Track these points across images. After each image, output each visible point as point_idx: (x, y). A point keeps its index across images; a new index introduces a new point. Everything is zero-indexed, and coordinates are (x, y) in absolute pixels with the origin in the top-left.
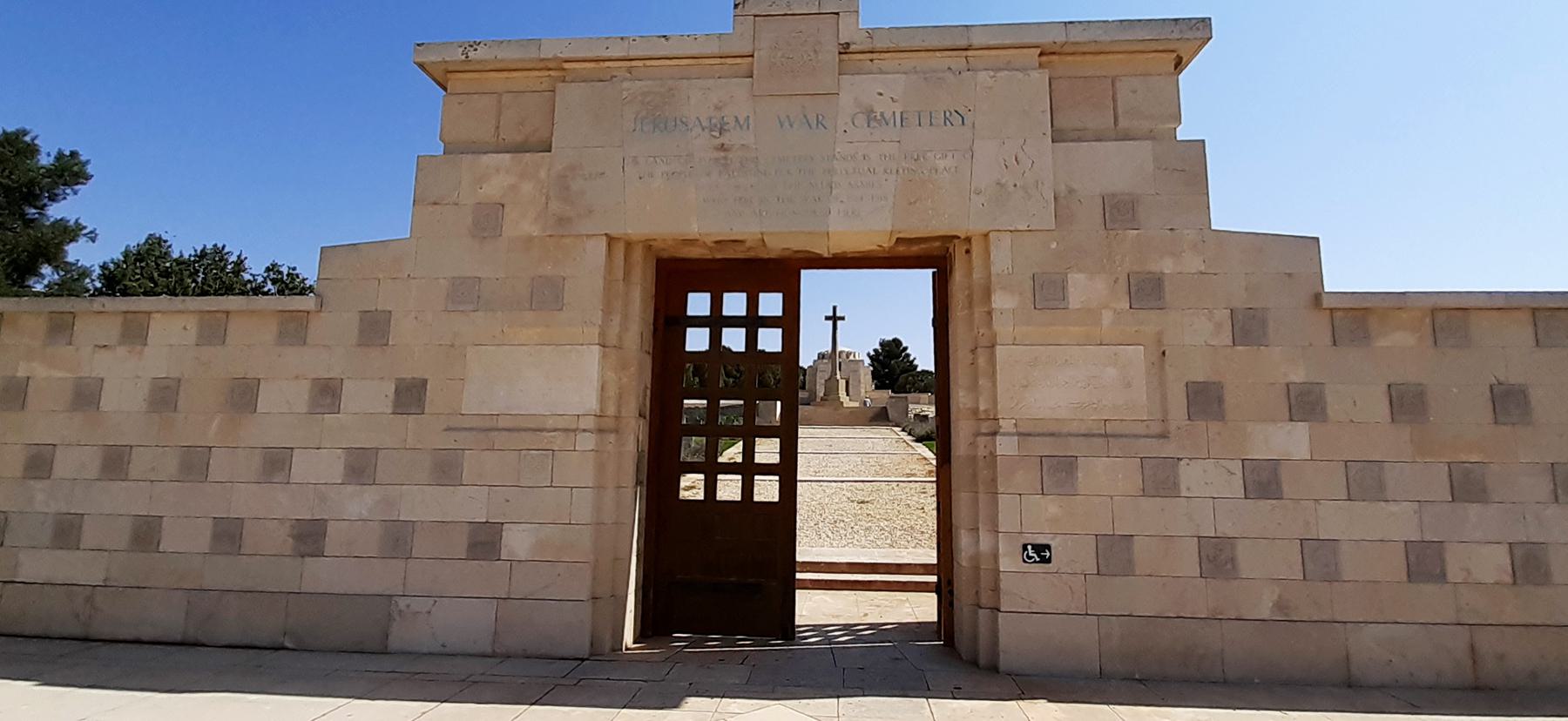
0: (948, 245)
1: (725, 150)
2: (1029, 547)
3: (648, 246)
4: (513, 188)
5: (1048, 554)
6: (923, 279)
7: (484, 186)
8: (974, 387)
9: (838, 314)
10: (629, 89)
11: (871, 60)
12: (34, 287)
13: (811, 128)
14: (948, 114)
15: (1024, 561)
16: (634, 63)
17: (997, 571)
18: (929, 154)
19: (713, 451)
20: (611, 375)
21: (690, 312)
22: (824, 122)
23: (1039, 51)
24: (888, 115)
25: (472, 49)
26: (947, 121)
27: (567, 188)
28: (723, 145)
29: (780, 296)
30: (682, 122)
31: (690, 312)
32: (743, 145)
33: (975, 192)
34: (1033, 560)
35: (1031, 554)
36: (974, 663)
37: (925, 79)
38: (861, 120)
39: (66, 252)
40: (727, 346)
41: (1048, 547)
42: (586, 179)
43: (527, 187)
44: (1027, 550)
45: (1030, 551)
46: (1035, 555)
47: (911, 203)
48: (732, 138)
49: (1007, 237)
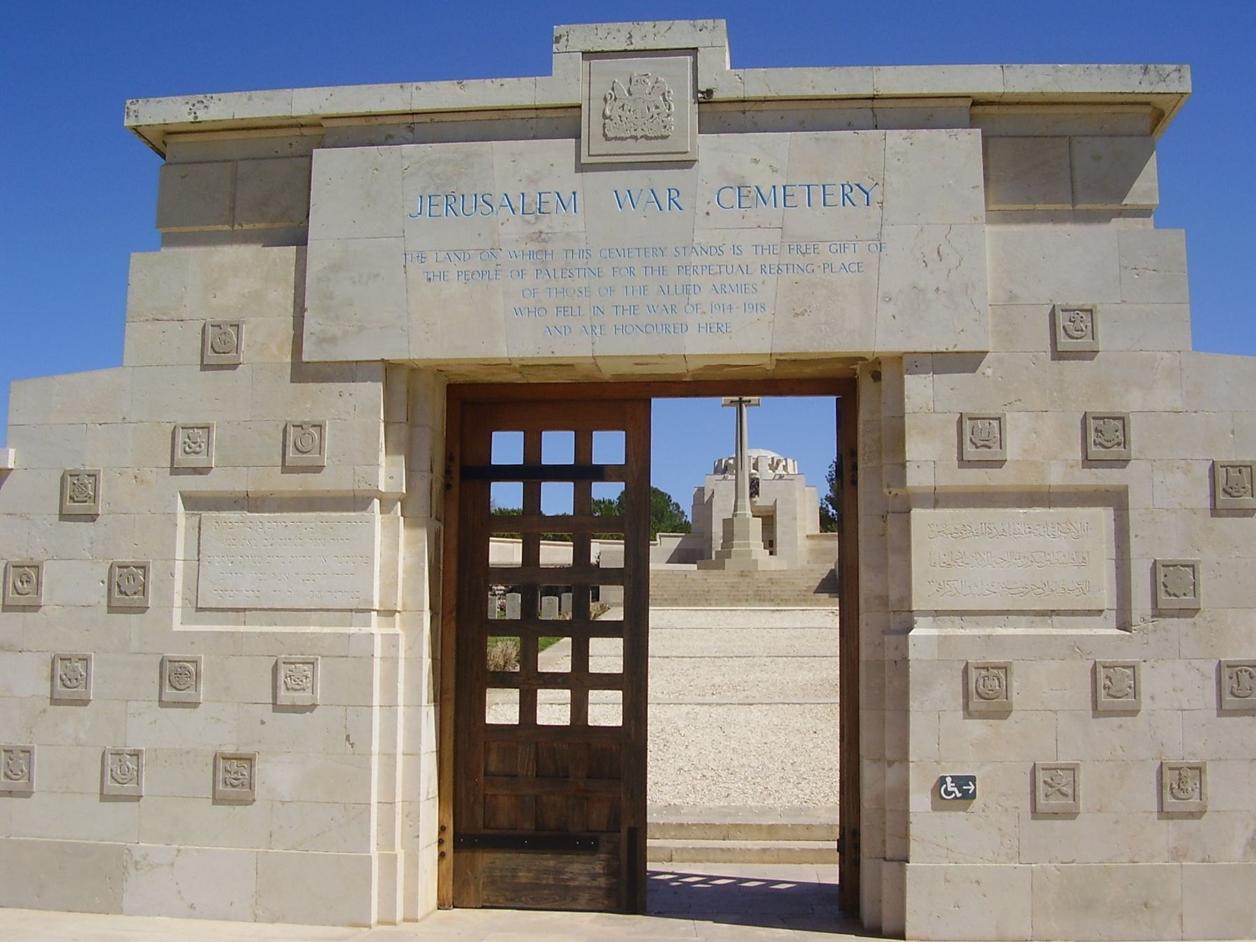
0: (854, 367)
1: (544, 241)
2: (949, 780)
3: (438, 370)
5: (972, 787)
6: (826, 406)
7: (218, 294)
11: (744, 112)
14: (847, 189)
16: (417, 119)
18: (821, 246)
19: (528, 656)
21: (547, 436)
23: (969, 102)
25: (202, 106)
29: (621, 435)
31: (547, 436)
32: (568, 234)
34: (954, 795)
35: (950, 789)
38: (730, 196)
40: (654, 487)
41: (973, 779)
42: (354, 282)
44: (946, 783)
45: (949, 784)
46: (955, 789)
48: (554, 223)
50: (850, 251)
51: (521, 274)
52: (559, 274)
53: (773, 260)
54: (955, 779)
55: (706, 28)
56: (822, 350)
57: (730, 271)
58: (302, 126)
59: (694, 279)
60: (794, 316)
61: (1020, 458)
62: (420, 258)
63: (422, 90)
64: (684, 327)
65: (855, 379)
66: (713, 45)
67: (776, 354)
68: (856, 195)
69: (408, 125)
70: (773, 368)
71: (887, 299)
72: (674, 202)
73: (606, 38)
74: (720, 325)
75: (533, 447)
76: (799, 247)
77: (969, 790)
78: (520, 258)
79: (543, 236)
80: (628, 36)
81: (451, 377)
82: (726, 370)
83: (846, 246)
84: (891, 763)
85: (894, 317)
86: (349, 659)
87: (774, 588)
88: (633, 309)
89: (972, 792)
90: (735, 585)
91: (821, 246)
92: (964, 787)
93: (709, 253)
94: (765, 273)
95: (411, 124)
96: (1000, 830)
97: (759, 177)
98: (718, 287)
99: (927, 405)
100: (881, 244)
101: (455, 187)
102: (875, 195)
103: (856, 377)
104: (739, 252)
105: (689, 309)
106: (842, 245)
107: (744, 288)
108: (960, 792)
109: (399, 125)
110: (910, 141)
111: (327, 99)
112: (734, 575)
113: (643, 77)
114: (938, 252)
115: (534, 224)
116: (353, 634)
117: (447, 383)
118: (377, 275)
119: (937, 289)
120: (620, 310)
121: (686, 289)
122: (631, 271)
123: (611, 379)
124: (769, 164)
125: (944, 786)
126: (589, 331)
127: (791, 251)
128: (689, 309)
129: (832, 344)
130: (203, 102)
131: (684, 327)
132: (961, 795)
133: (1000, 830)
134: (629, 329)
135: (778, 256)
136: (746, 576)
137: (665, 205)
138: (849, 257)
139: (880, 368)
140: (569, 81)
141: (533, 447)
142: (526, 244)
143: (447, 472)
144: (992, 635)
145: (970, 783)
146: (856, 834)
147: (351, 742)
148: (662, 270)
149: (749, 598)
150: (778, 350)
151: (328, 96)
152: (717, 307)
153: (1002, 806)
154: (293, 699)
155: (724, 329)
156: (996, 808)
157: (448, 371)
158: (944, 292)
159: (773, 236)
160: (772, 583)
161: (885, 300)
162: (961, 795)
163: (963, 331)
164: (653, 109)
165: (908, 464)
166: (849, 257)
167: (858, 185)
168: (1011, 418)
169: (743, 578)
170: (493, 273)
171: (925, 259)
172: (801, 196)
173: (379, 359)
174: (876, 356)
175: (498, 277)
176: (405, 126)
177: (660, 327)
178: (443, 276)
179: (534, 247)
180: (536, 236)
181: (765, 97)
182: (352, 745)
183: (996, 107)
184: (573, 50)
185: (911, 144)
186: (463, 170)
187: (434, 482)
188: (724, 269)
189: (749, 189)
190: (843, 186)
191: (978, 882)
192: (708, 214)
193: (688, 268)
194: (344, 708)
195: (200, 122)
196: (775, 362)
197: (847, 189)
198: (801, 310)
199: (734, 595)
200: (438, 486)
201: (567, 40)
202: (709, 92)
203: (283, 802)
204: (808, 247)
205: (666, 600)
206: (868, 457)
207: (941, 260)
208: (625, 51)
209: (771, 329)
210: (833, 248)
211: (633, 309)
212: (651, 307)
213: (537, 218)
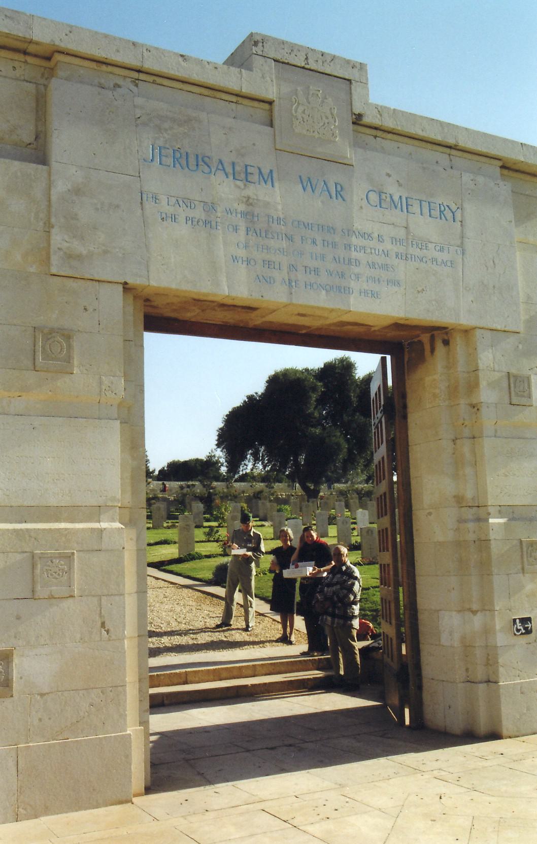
5: (530, 625)
12: (252, 597)
15: (515, 634)
18: (430, 245)
22: (341, 193)
23: (500, 163)
30: (203, 161)
35: (519, 628)
37: (424, 168)
39: (214, 574)
41: (529, 619)
44: (516, 624)
47: (419, 292)
49: (488, 334)
50: (446, 251)
57: (377, 252)
63: (151, 53)
69: (133, 80)
72: (340, 194)
74: (373, 293)
78: (234, 214)
80: (305, 57)
95: (136, 79)
108: (524, 629)
109: (125, 77)
115: (243, 189)
116: (105, 529)
118: (118, 206)
122: (314, 242)
126: (287, 283)
137: (334, 195)
138: (445, 256)
142: (238, 204)
147: (106, 629)
148: (334, 245)
151: (68, 33)
152: (371, 278)
154: (51, 593)
159: (402, 233)
164: (324, 118)
167: (448, 206)
170: (213, 224)
176: (130, 80)
178: (174, 218)
182: (108, 632)
183: (507, 171)
188: (373, 251)
190: (440, 204)
194: (95, 600)
203: (42, 695)
211: (316, 271)
213: (245, 185)
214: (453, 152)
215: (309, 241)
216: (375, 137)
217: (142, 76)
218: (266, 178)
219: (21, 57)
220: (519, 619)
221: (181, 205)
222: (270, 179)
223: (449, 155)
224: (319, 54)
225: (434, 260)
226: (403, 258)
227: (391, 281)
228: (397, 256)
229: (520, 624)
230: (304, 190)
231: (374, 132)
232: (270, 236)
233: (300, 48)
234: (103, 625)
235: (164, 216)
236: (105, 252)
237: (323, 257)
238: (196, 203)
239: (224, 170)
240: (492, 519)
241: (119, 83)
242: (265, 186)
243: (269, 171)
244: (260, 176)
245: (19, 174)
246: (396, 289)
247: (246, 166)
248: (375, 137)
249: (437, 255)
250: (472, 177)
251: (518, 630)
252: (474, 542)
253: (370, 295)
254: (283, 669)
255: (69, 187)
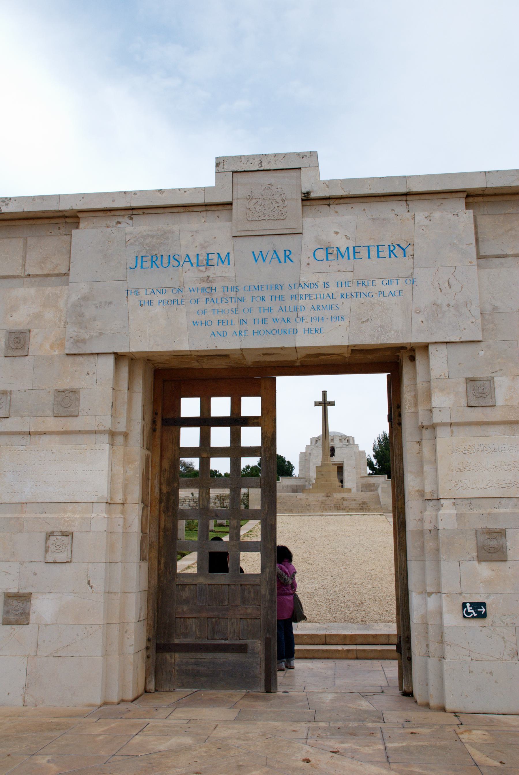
1: (210, 281)
4: (38, 316)
5: (484, 610)
7: (14, 314)
8: (421, 473)
9: (329, 399)
10: (131, 234)
13: (280, 262)
15: (464, 617)
17: (441, 625)
18: (377, 281)
20: (119, 469)
23: (465, 195)
24: (343, 250)
25: (4, 204)
26: (391, 253)
27: (82, 315)
28: (209, 277)
31: (184, 413)
33: (416, 311)
34: (472, 615)
35: (469, 611)
36: (427, 705)
38: (321, 254)
41: (484, 604)
43: (49, 315)
44: (466, 607)
45: (469, 608)
46: (473, 611)
51: (197, 301)
52: (219, 301)
53: (348, 290)
54: (472, 604)
55: (306, 156)
56: (379, 342)
57: (322, 296)
58: (66, 217)
59: (301, 302)
60: (361, 323)
61: (504, 404)
62: (136, 293)
64: (295, 331)
65: (398, 362)
66: (310, 166)
67: (351, 346)
68: (397, 251)
69: (130, 216)
70: (349, 355)
71: (418, 312)
73: (247, 163)
75: (205, 407)
76: (364, 282)
77: (482, 611)
78: (196, 291)
79: (210, 279)
80: (259, 162)
81: (156, 365)
82: (321, 358)
83: (392, 281)
84: (430, 594)
85: (422, 322)
86: (91, 533)
87: (345, 503)
88: (264, 321)
89: (484, 613)
90: (323, 501)
91: (377, 281)
92: (479, 610)
93: (309, 287)
94: (344, 298)
95: (131, 215)
96: (503, 638)
97: (341, 242)
98: (315, 307)
99: (445, 374)
100: (413, 279)
101: (157, 251)
102: (409, 251)
103: (399, 361)
104: (327, 286)
105: (298, 320)
106: (390, 281)
107: (331, 307)
110: (429, 219)
111: (80, 201)
112: (323, 496)
113: (269, 186)
114: (449, 283)
117: (154, 369)
118: (111, 303)
119: (448, 305)
120: (256, 321)
121: (296, 309)
123: (252, 365)
124: (345, 235)
125: (465, 609)
127: (359, 284)
128: (298, 320)
129: (385, 339)
130: (5, 202)
131: (295, 331)
132: (476, 615)
133: (503, 638)
134: (262, 332)
135: (351, 288)
136: (330, 496)
138: (394, 287)
139: (415, 354)
140: (225, 189)
141: (205, 407)
143: (154, 422)
144: (491, 513)
145: (482, 607)
146: (408, 640)
147: (91, 585)
148: (281, 298)
149: (331, 508)
150: (351, 343)
153: (504, 622)
155: (319, 331)
156: (500, 624)
157: (154, 360)
158: (453, 306)
160: (344, 500)
161: (416, 312)
162: (476, 615)
163: (465, 329)
165: (434, 409)
166: (394, 287)
167: (398, 245)
168: (498, 380)
169: (328, 498)
170: (180, 301)
171: (440, 287)
172: (364, 253)
173: (111, 351)
174: (412, 345)
175: (183, 303)
176: (127, 216)
177: (280, 331)
178: (150, 303)
179: (205, 285)
180: (205, 279)
181: (342, 195)
182: (91, 587)
183: (481, 198)
184: (227, 171)
185: (430, 220)
186: (162, 241)
187: (145, 426)
188: (318, 296)
189: (333, 249)
190: (389, 245)
191: (491, 673)
192: (308, 264)
193: (297, 296)
195: (3, 213)
196: (350, 351)
197: (392, 248)
198: (366, 319)
199: (323, 507)
200: (148, 429)
201: (224, 165)
202: (308, 193)
203: (46, 625)
204: (369, 282)
205: (286, 510)
206: (409, 406)
207: (450, 288)
208: (258, 171)
209: (348, 330)
210: (384, 283)
211: (264, 321)
212: (275, 319)
213: (206, 268)
214: (409, 198)
215: (258, 299)
216: (329, 205)
217: (135, 212)
218: (223, 260)
219: (63, 220)
220: (469, 603)
221: (156, 293)
222: (227, 260)
223: (406, 201)
224: (272, 156)
225: (381, 293)
226: (348, 297)
227: (335, 318)
228: (342, 296)
229: (471, 608)
230: (256, 261)
231: (327, 202)
232: (225, 301)
233: (254, 157)
234: (89, 583)
235: (142, 303)
236: (101, 334)
237: (270, 309)
238: (166, 289)
239: (190, 261)
240: (259, 497)
241: (119, 221)
242: (223, 266)
243: (226, 254)
244: (219, 258)
245: (51, 295)
246: (340, 323)
247: (208, 254)
248: (329, 205)
249: (387, 289)
250: (426, 214)
251: (468, 613)
252: (430, 531)
253: (314, 332)
254: (337, 655)
255: (79, 297)
